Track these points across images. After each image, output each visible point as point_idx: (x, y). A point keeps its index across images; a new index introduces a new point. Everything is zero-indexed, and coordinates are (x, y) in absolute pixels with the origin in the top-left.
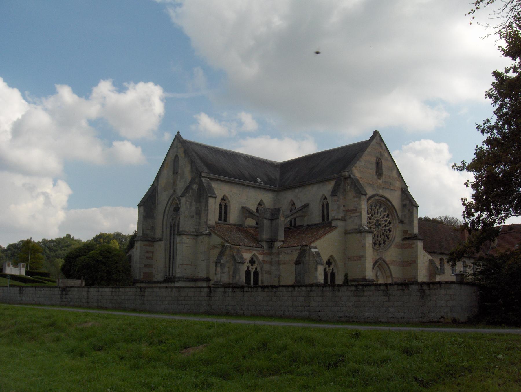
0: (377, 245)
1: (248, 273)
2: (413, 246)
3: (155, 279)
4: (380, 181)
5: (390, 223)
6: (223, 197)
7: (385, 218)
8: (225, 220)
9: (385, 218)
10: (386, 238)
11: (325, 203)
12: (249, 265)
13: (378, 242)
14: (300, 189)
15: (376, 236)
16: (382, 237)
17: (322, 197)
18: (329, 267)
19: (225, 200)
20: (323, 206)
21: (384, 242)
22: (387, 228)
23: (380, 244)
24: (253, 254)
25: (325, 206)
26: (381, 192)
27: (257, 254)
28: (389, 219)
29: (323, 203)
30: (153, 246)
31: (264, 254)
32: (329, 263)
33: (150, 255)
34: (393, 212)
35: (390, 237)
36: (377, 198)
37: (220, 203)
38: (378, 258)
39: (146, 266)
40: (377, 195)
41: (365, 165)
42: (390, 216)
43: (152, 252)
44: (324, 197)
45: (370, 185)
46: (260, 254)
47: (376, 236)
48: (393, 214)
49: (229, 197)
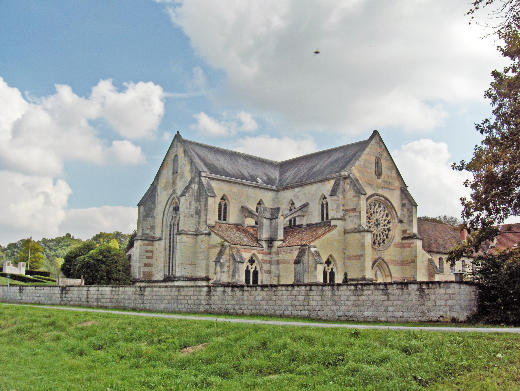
0: (377, 245)
1: (247, 272)
2: (412, 245)
3: (154, 279)
4: (380, 181)
5: (389, 223)
6: (223, 197)
7: (384, 218)
8: (225, 219)
9: (384, 218)
10: (385, 237)
11: (324, 203)
12: (249, 264)
13: (377, 242)
14: (299, 189)
15: (375, 235)
16: (382, 236)
17: (322, 196)
18: (328, 266)
19: (224, 200)
20: (322, 205)
21: (384, 241)
22: (386, 227)
23: (379, 244)
24: (252, 253)
25: (325, 206)
26: (380, 192)
27: (256, 253)
28: (388, 219)
29: (323, 202)
30: (153, 245)
31: (263, 253)
32: (328, 262)
33: (149, 254)
34: (392, 211)
35: (390, 236)
36: (376, 197)
37: (220, 202)
38: (377, 257)
39: (145, 265)
40: (377, 195)
41: (364, 164)
42: (389, 216)
43: (152, 252)
44: (323, 197)
45: (370, 184)
46: (260, 253)
47: (375, 235)
48: (393, 213)
49: (228, 196)
